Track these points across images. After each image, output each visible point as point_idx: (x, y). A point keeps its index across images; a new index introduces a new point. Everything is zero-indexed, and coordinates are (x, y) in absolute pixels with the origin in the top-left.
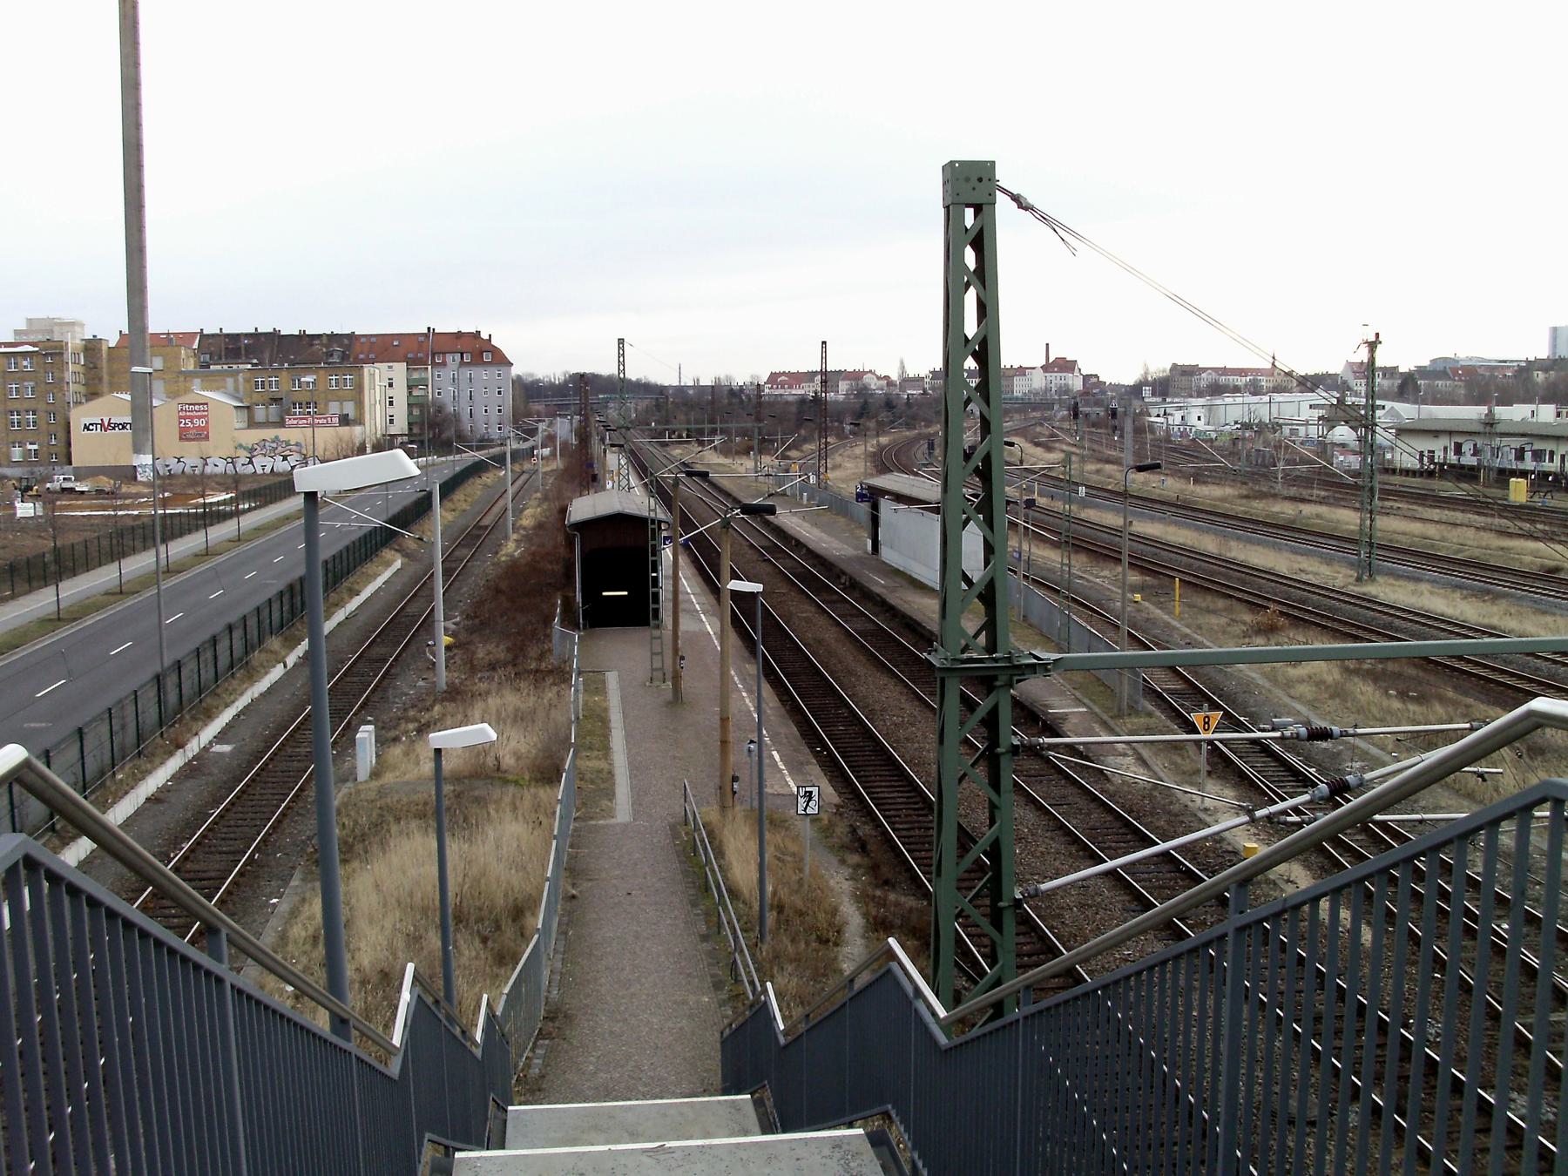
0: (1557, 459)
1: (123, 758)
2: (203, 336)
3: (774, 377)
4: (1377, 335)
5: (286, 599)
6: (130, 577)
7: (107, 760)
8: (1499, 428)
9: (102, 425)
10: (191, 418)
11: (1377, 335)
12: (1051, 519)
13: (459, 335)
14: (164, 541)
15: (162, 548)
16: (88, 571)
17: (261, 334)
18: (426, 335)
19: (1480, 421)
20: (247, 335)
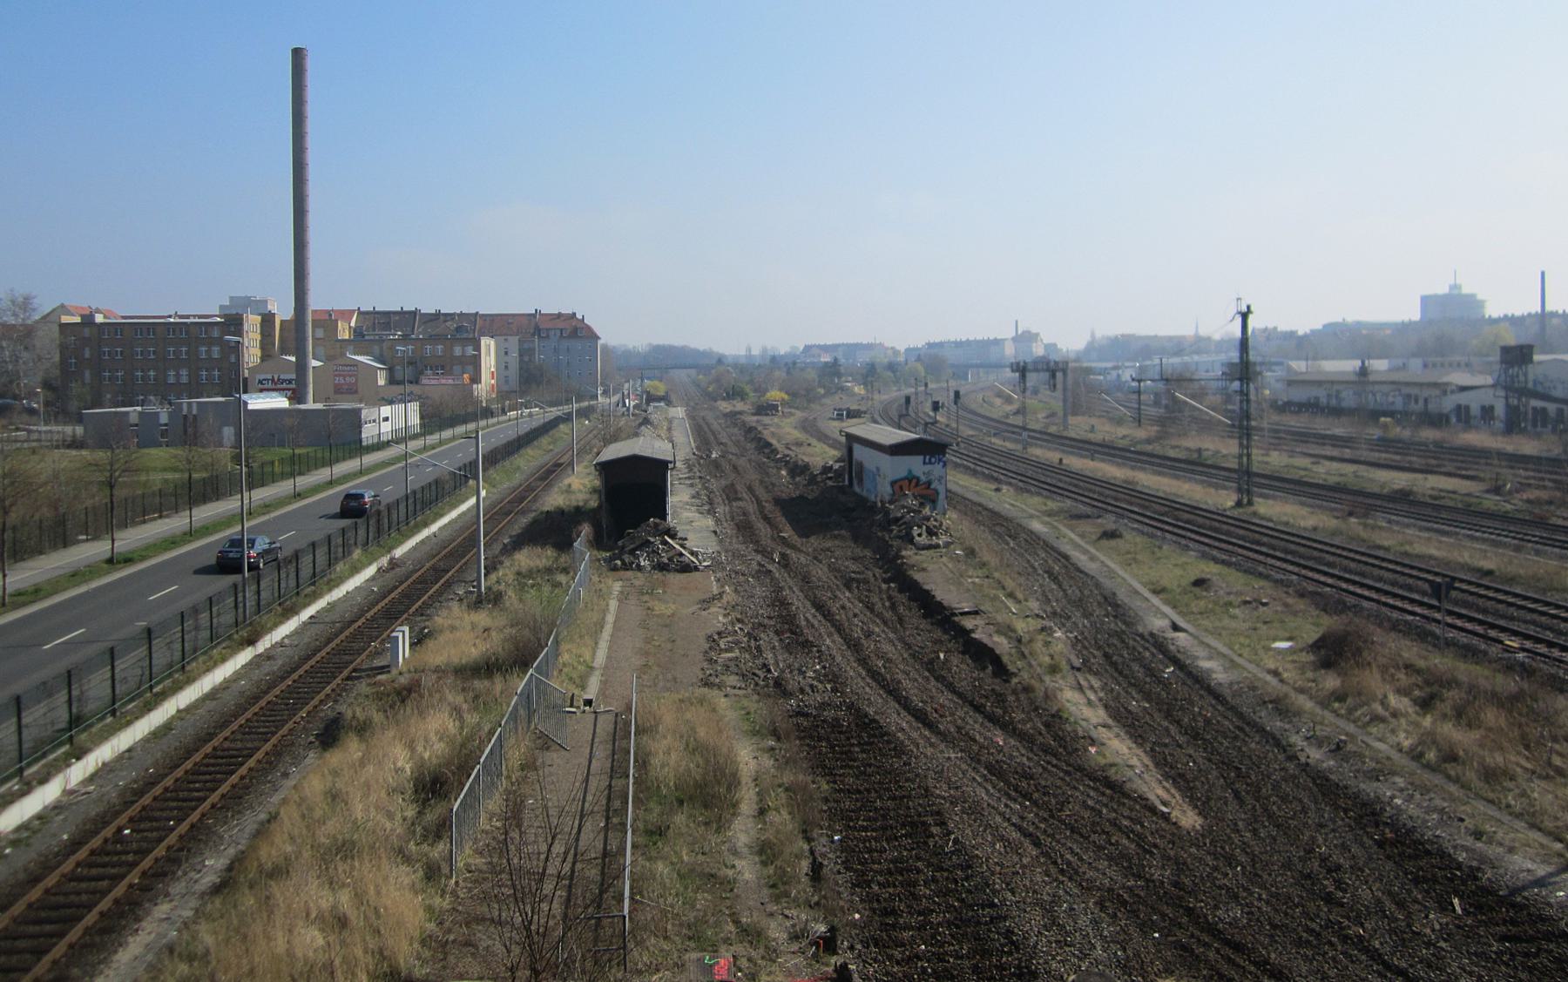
0: (1421, 402)
1: (195, 651)
2: (360, 313)
3: (808, 348)
4: (1248, 307)
5: (434, 488)
6: (258, 503)
7: (178, 655)
8: (1371, 378)
9: (273, 380)
10: (344, 376)
11: (1248, 307)
12: (1049, 480)
13: (559, 315)
14: (251, 488)
15: (246, 495)
16: (65, 546)
17: (378, 313)
18: (533, 316)
19: (1355, 373)
20: (395, 313)
